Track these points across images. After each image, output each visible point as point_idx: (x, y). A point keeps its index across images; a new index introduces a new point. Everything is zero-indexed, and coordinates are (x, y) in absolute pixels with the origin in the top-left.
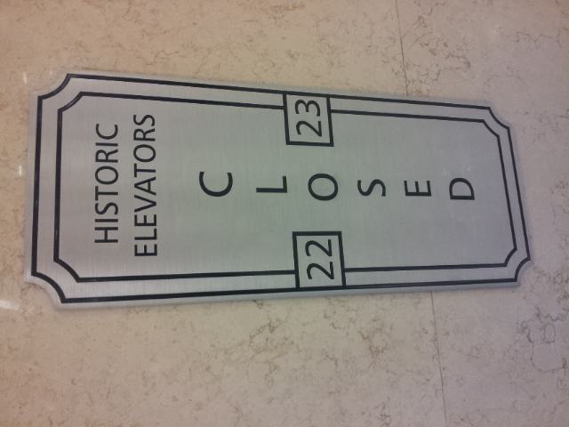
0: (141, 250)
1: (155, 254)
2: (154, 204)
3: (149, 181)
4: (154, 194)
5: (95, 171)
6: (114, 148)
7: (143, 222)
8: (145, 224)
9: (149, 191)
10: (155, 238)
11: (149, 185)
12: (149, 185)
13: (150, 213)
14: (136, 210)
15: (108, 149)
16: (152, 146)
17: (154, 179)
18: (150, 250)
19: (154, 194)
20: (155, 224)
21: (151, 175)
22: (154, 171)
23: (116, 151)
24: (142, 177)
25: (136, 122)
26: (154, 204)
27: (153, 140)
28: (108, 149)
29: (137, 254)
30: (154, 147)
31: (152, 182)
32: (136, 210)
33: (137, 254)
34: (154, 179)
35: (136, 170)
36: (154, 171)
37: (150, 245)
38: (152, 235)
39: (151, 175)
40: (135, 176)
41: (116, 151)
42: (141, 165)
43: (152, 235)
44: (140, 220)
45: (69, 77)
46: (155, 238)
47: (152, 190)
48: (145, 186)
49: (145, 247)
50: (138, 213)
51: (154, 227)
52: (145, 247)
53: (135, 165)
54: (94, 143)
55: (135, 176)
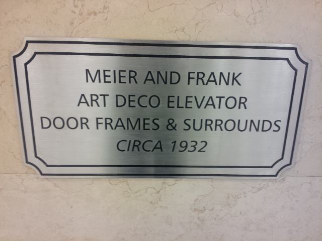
0: (171, 99)
1: (169, 107)
2: (199, 107)
3: (213, 105)
4: (205, 108)
5: (179, 73)
6: (214, 128)
7: (188, 101)
8: (187, 102)
9: (207, 104)
10: (178, 107)
11: (159, 148)
12: (159, 148)
13: (194, 104)
14: (195, 97)
15: (213, 126)
16: (236, 107)
17: (214, 108)
18: (171, 104)
19: (205, 108)
20: (186, 107)
21: (217, 106)
22: (219, 108)
23: (212, 130)
24: (216, 101)
25: (277, 131)
26: (199, 107)
27: (239, 108)
28: (213, 126)
29: (97, 119)
30: (234, 130)
31: (212, 106)
32: (195, 97)
33: (97, 119)
34: (214, 108)
35: (220, 98)
36: (219, 108)
37: (175, 104)
38: (180, 106)
39: (217, 106)
40: (217, 97)
41: (212, 130)
42: (223, 101)
43: (180, 106)
44: (189, 99)
45: (307, 64)
46: (178, 107)
47: (207, 106)
48: (210, 102)
49: (173, 102)
50: (194, 98)
51: (184, 106)
52: (173, 102)
53: (224, 97)
54: (215, 109)
55: (217, 97)
